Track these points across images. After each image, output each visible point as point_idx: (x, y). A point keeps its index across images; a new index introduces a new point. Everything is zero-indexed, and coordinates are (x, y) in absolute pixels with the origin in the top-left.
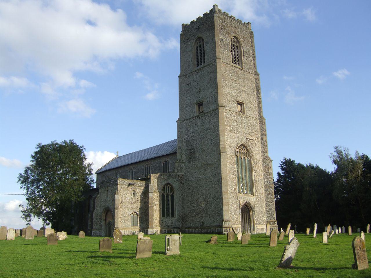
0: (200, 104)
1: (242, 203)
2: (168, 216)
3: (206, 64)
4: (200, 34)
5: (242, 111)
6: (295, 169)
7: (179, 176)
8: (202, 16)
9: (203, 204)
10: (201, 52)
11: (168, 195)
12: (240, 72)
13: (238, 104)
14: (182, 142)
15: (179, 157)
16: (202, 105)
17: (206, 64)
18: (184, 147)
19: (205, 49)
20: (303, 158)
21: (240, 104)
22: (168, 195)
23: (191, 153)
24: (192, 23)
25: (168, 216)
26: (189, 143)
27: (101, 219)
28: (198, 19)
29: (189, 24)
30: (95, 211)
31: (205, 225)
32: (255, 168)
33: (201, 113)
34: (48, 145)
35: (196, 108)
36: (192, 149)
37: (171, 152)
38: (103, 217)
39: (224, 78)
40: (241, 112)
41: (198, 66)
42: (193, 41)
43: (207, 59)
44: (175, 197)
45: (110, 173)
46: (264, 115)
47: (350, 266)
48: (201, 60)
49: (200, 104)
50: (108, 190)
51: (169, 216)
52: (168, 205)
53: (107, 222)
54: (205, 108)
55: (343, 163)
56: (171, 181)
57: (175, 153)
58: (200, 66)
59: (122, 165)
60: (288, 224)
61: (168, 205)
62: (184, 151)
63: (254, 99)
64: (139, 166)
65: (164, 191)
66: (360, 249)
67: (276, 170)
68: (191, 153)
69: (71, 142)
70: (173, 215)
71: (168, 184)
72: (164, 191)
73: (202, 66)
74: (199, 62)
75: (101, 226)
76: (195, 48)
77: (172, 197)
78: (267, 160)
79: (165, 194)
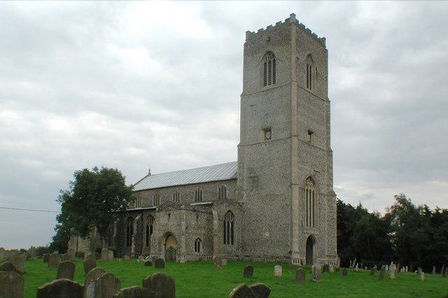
0: (267, 130)
4: (270, 48)
8: (274, 25)
9: (267, 234)
10: (270, 68)
15: (239, 183)
18: (245, 174)
19: (277, 67)
21: (310, 133)
23: (255, 180)
24: (261, 31)
25: (228, 243)
26: (251, 170)
27: (159, 244)
28: (268, 27)
29: (256, 32)
30: (152, 235)
32: (294, 201)
34: (32, 249)
35: (262, 133)
37: (229, 178)
38: (163, 242)
41: (265, 85)
42: (261, 55)
45: (147, 193)
50: (169, 215)
52: (228, 236)
53: (168, 246)
55: (405, 210)
57: (233, 180)
58: (265, 88)
59: (165, 185)
64: (188, 190)
68: (255, 180)
70: (232, 244)
75: (160, 250)
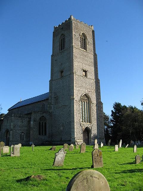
1: (84, 128)
2: (43, 134)
3: (65, 49)
4: (63, 32)
5: (86, 75)
6: (120, 108)
7: (50, 112)
9: (62, 128)
11: (42, 123)
12: (85, 54)
13: (83, 71)
14: (52, 92)
16: (63, 72)
17: (65, 49)
20: (126, 103)
21: (84, 71)
22: (42, 123)
25: (43, 134)
27: (4, 136)
31: (63, 139)
33: (62, 77)
35: (59, 74)
36: (57, 97)
39: (76, 57)
40: (85, 76)
43: (66, 46)
44: (47, 124)
46: (99, 78)
47: (90, 167)
48: (63, 47)
49: (62, 72)
51: (40, 135)
54: (64, 74)
56: (44, 115)
57: (48, 99)
60: (120, 140)
61: (43, 128)
62: (53, 98)
63: (93, 68)
65: (40, 121)
66: (97, 156)
67: (108, 110)
68: (57, 98)
69: (120, 104)
70: (45, 134)
71: (43, 116)
72: (40, 121)
73: (64, 50)
74: (62, 48)
76: (61, 40)
77: (45, 124)
78: (99, 105)
79: (41, 122)
